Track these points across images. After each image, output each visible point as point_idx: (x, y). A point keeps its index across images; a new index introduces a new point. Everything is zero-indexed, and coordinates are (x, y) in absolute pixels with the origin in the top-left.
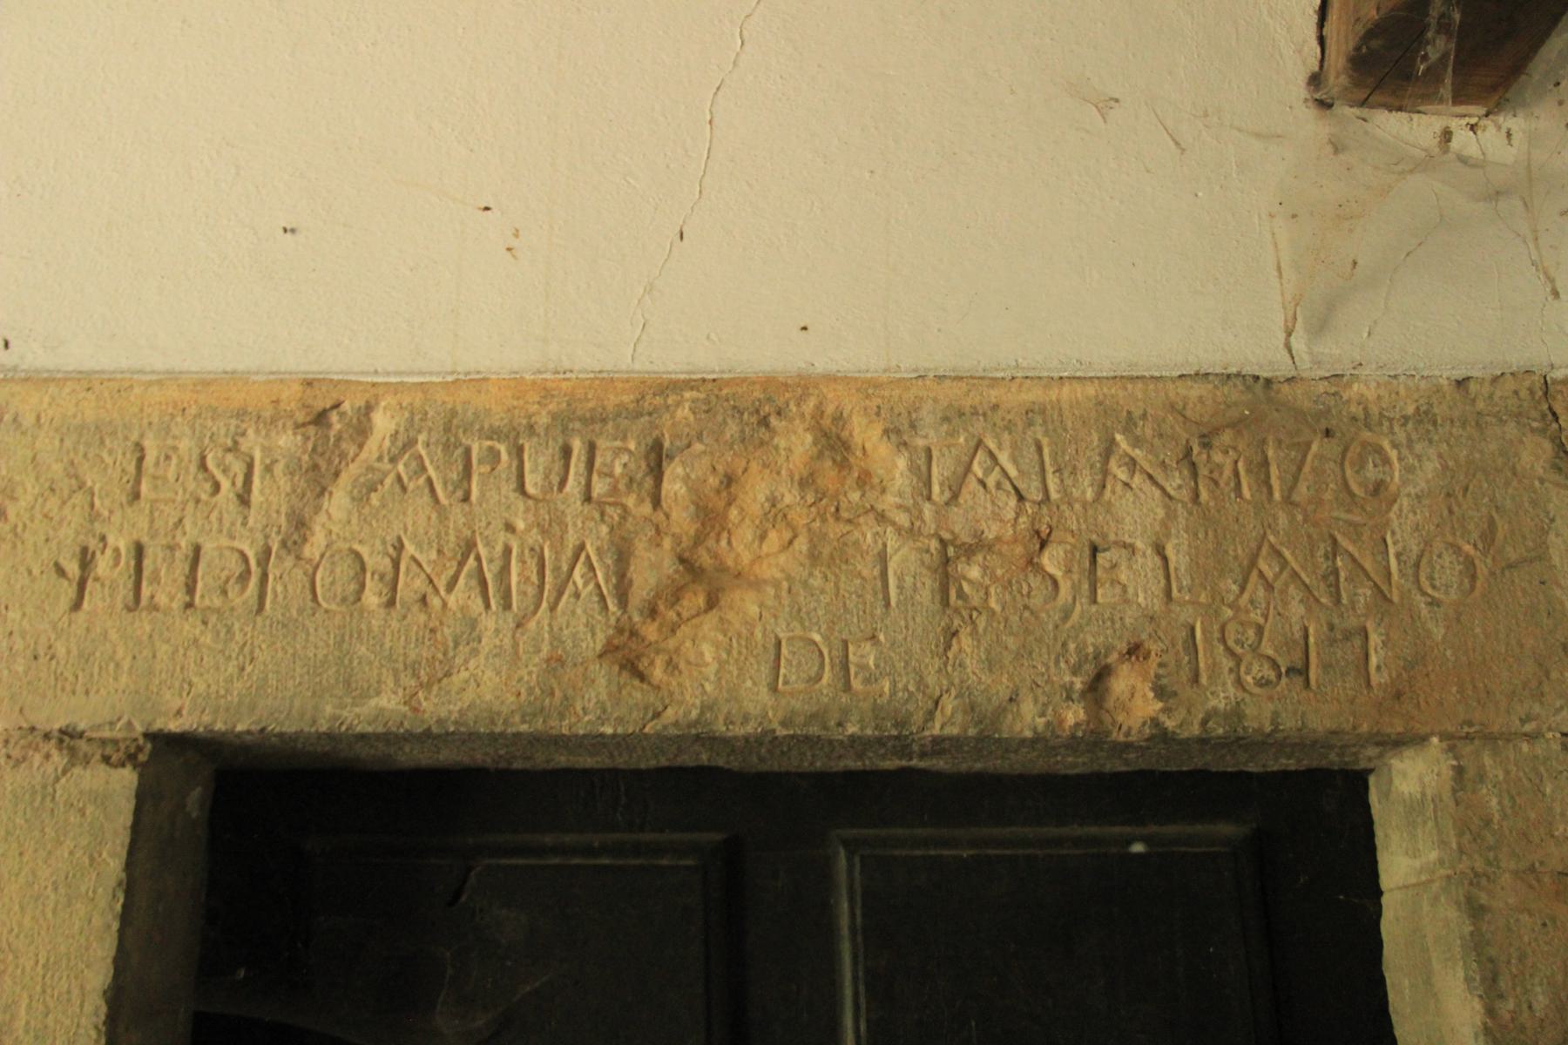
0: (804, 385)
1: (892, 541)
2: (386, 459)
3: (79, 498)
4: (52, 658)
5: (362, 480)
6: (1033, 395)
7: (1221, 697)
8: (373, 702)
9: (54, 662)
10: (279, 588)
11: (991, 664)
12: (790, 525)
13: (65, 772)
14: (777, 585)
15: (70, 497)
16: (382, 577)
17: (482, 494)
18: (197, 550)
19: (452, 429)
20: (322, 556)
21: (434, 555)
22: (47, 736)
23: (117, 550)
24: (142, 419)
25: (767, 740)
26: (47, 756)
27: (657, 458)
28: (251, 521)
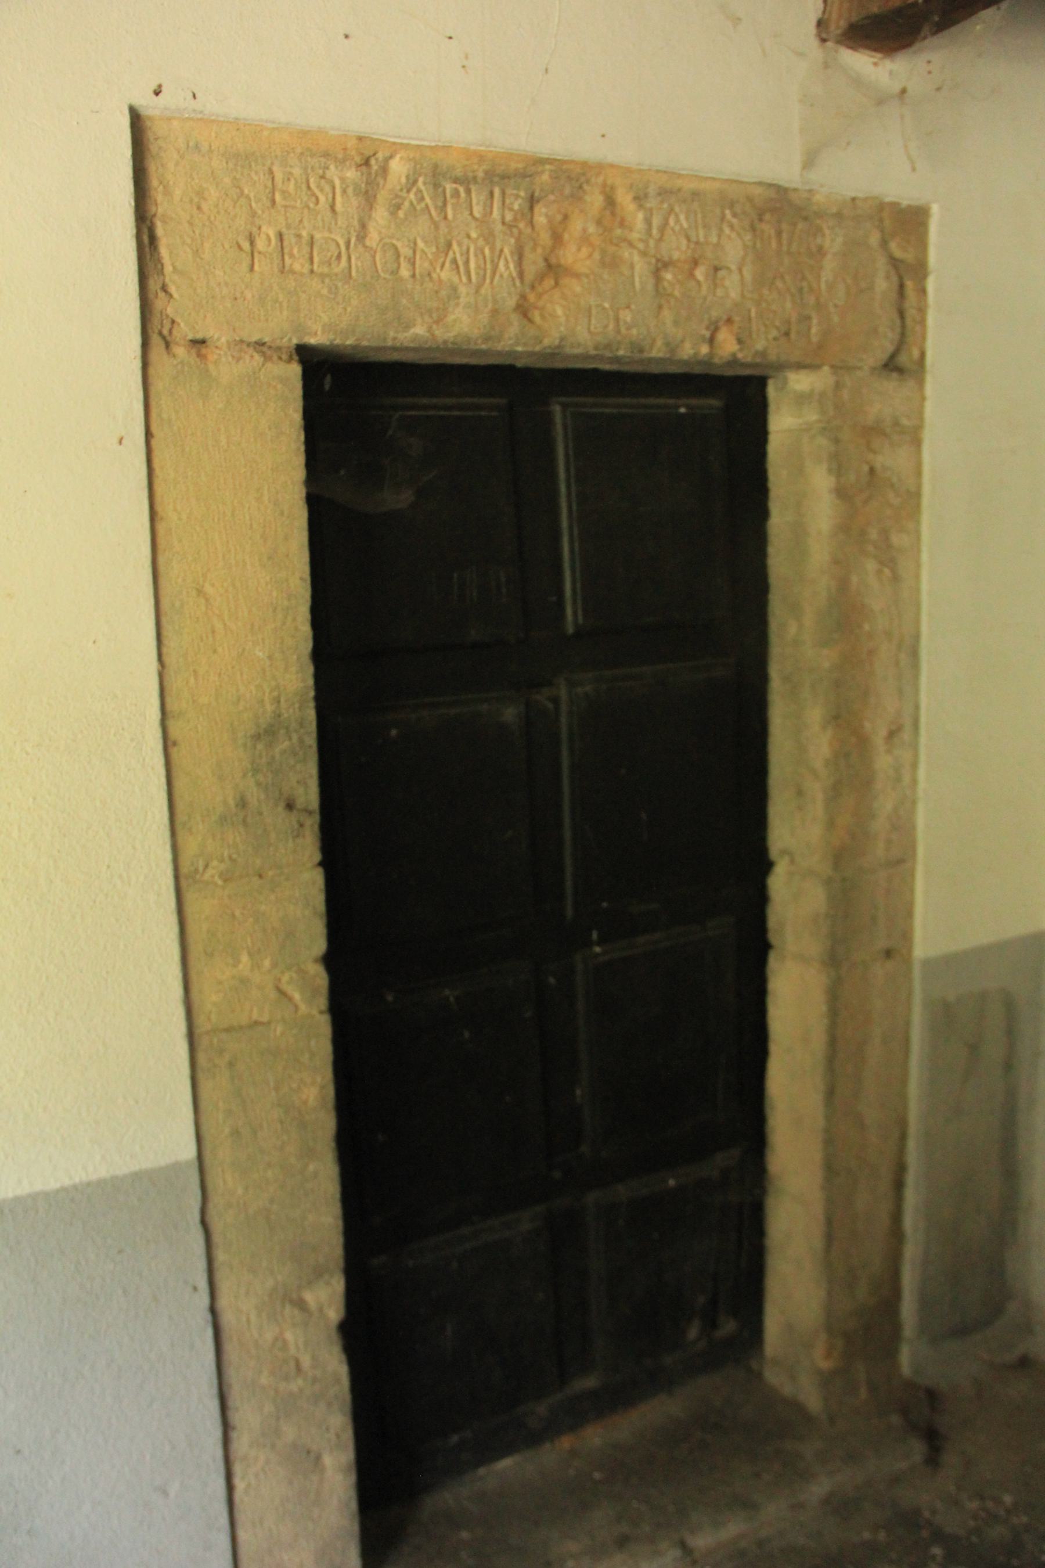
0: (600, 167)
1: (636, 258)
2: (405, 191)
3: (243, 201)
4: (245, 300)
5: (394, 202)
6: (693, 185)
7: (759, 346)
8: (412, 331)
9: (246, 302)
10: (359, 264)
11: (676, 323)
12: (591, 245)
13: (263, 365)
14: (587, 276)
15: (238, 200)
16: (409, 260)
17: (454, 215)
18: (312, 237)
19: (437, 175)
20: (378, 245)
21: (434, 249)
22: (249, 345)
23: (268, 236)
24: (271, 153)
25: (586, 357)
26: (252, 357)
27: (532, 201)
28: (339, 223)
